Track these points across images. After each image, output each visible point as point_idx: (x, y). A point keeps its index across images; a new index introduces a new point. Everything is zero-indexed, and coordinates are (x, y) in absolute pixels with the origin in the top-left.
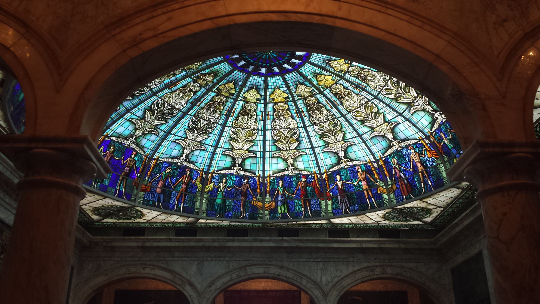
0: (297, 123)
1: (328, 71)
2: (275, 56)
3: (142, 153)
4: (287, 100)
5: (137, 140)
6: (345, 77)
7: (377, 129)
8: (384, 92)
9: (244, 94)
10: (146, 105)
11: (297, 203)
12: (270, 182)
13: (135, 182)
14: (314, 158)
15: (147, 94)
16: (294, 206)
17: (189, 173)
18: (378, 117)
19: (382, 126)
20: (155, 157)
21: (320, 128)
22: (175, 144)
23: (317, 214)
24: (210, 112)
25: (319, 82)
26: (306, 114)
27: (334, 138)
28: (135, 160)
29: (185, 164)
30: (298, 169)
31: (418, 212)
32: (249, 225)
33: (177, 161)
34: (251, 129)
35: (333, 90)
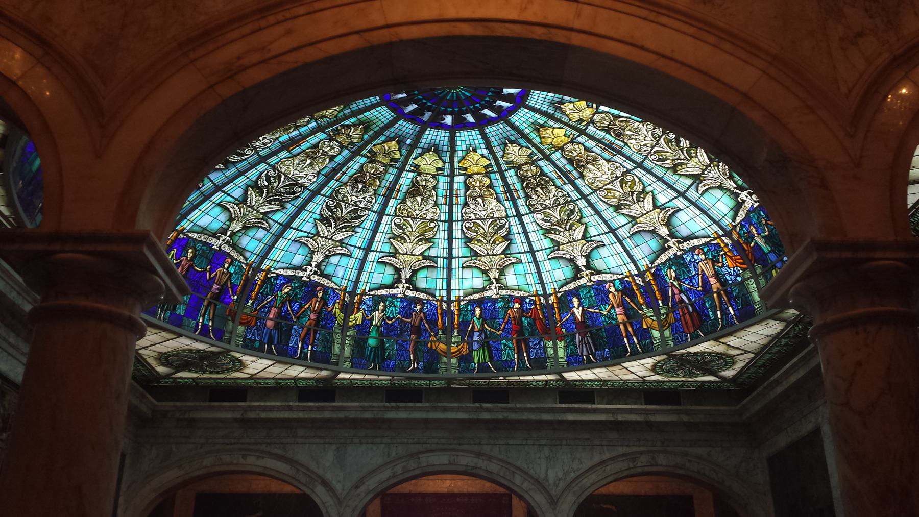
0: (506, 208)
1: (557, 120)
2: (468, 94)
3: (242, 260)
4: (488, 170)
5: (233, 238)
6: (588, 131)
7: (642, 219)
8: (653, 157)
9: (414, 159)
10: (248, 178)
11: (505, 345)
12: (459, 310)
13: (230, 310)
14: (534, 269)
15: (250, 160)
16: (501, 350)
17: (321, 294)
18: (644, 199)
19: (649, 213)
20: (264, 267)
21: (545, 219)
22: (298, 245)
23: (540, 365)
24: (357, 191)
25: (543, 140)
26: (521, 193)
27: (568, 235)
28: (230, 273)
29: (315, 278)
30: (507, 288)
31: (711, 361)
32: (424, 383)
33: (301, 274)
34: (427, 220)
35: (566, 153)
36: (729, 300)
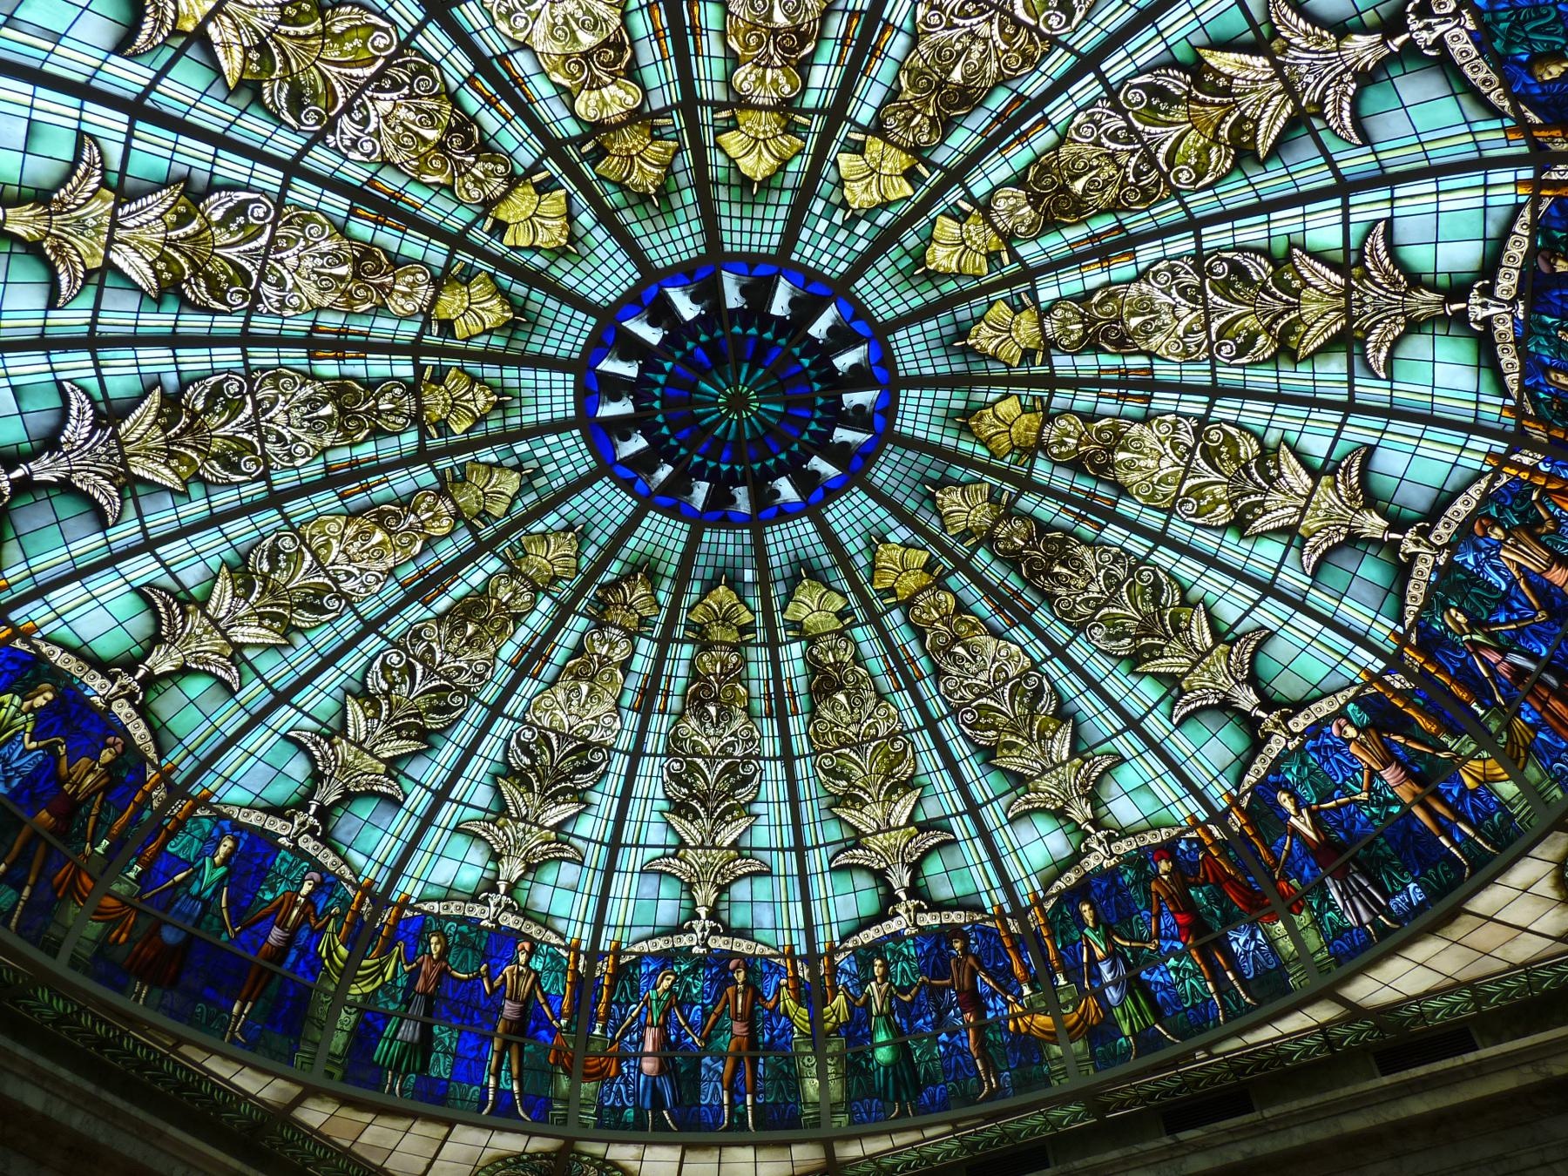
0: (1022, 647)
2: (778, 409)
3: (555, 940)
4: (936, 573)
7: (1310, 523)
8: (1225, 350)
11: (1176, 970)
12: (1048, 924)
13: (558, 1052)
14: (1160, 767)
17: (742, 975)
18: (1279, 469)
19: (1315, 498)
20: (604, 946)
22: (654, 879)
25: (992, 446)
26: (1029, 596)
28: (536, 971)
29: (718, 943)
30: (1125, 833)
33: (685, 941)
35: (1055, 451)
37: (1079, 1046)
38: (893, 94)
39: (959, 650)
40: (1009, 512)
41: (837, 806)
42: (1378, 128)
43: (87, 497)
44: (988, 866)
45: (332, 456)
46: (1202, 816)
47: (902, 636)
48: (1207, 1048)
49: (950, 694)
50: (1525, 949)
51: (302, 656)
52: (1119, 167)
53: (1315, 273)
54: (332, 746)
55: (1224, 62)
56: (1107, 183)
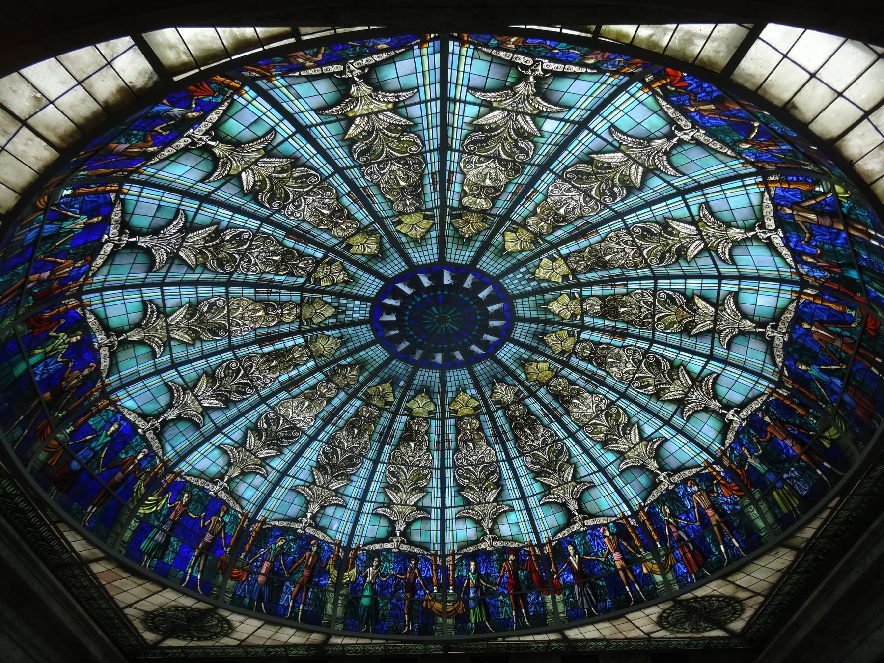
1: (542, 354)
3: (238, 509)
8: (636, 384)
11: (502, 601)
12: (454, 565)
13: (222, 562)
14: (526, 518)
15: (251, 400)
16: (498, 608)
20: (259, 518)
22: (294, 494)
23: (539, 622)
26: (510, 435)
29: (310, 531)
30: (501, 538)
31: (719, 608)
32: (420, 647)
33: (296, 526)
36: (731, 530)
37: (450, 621)
38: (581, 251)
39: (471, 444)
40: (519, 401)
41: (388, 488)
42: (734, 347)
43: (153, 257)
44: (439, 533)
45: (265, 276)
46: (535, 542)
47: (450, 430)
48: (504, 638)
49: (458, 459)
50: (636, 634)
51: (195, 351)
52: (641, 312)
53: (684, 377)
54: (184, 394)
55: (700, 303)
56: (632, 314)
